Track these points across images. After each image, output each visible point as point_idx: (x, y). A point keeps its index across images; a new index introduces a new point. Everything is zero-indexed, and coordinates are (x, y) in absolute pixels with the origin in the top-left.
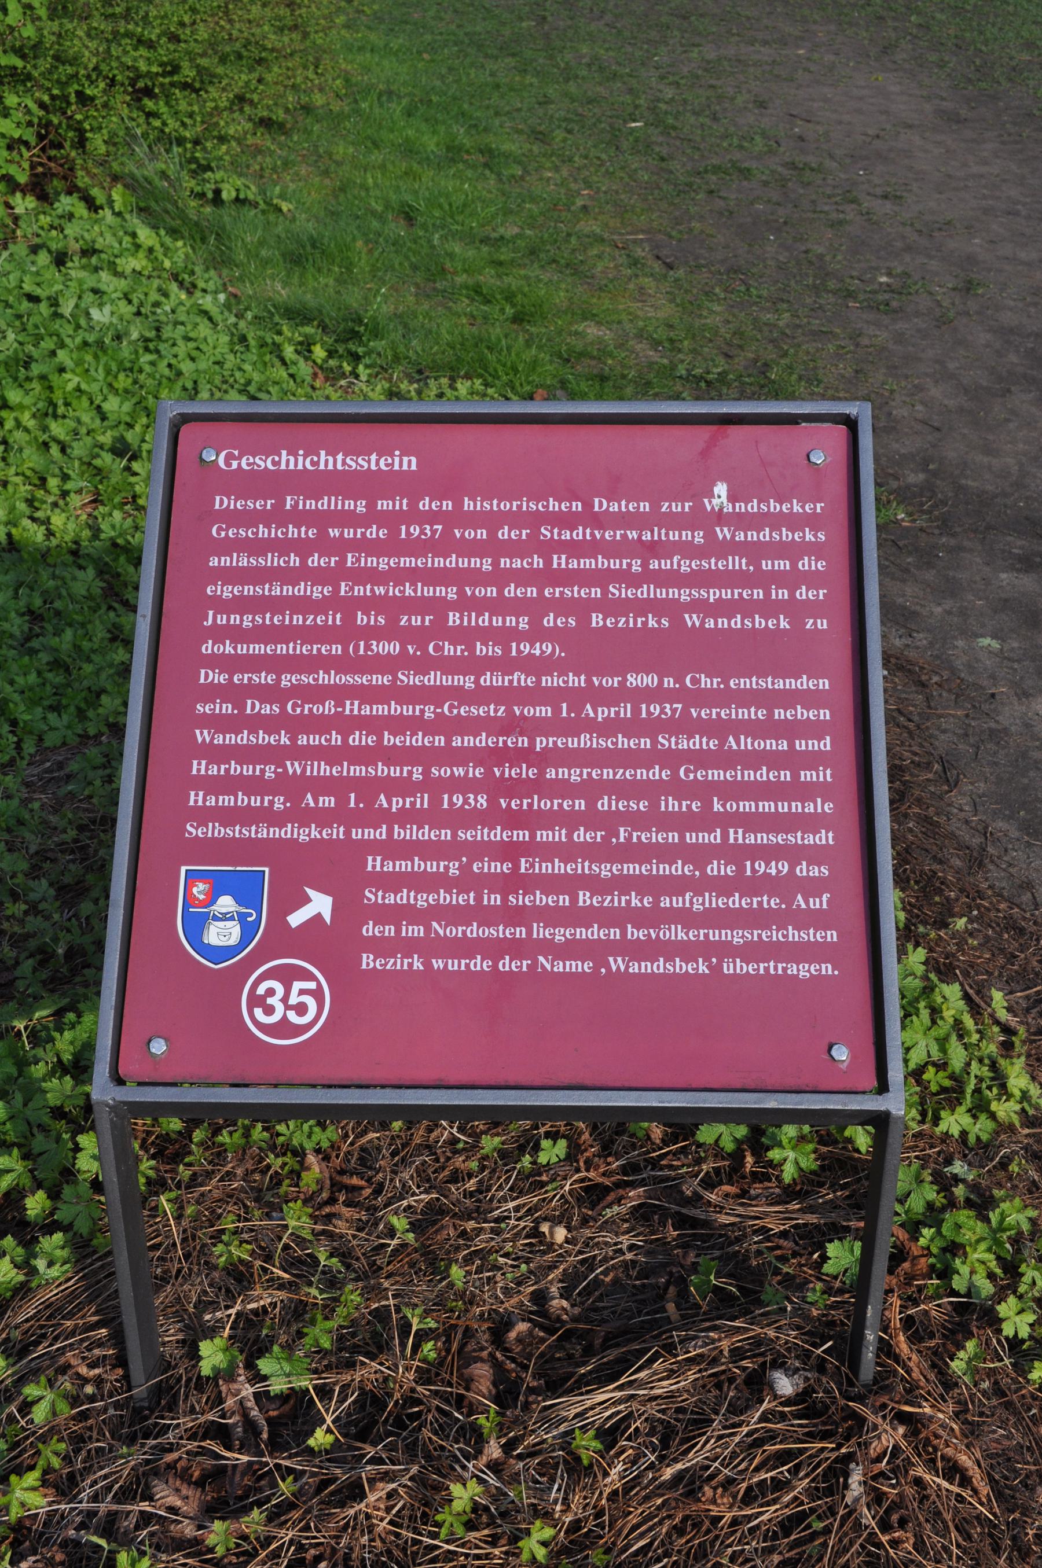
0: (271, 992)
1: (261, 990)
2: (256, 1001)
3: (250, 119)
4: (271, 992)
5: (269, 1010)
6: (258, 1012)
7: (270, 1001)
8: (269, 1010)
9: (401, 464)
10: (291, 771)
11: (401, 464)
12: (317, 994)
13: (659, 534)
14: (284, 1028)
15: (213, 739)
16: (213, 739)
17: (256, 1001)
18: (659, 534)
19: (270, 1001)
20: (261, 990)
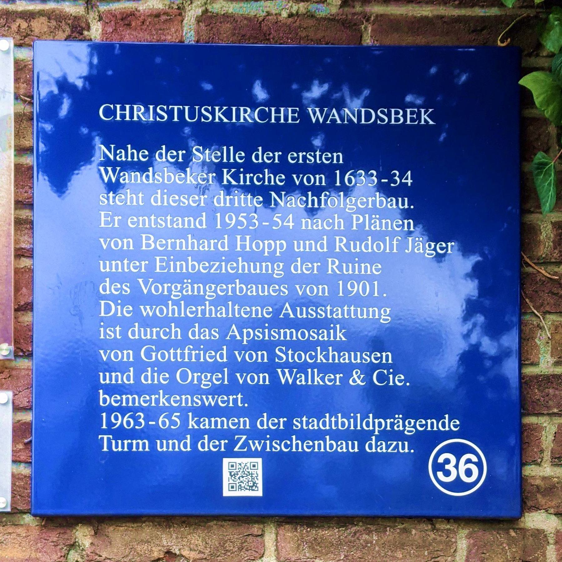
0: (447, 461)
1: (441, 460)
2: (438, 467)
3: (315, 11)
4: (447, 461)
5: (447, 473)
6: (440, 474)
7: (447, 467)
8: (447, 473)
9: (175, 268)
10: (253, 449)
11: (175, 268)
12: (479, 465)
13: (233, 310)
14: (458, 485)
15: (295, 379)
16: (295, 379)
17: (438, 467)
18: (233, 310)
19: (447, 467)
20: (441, 460)
